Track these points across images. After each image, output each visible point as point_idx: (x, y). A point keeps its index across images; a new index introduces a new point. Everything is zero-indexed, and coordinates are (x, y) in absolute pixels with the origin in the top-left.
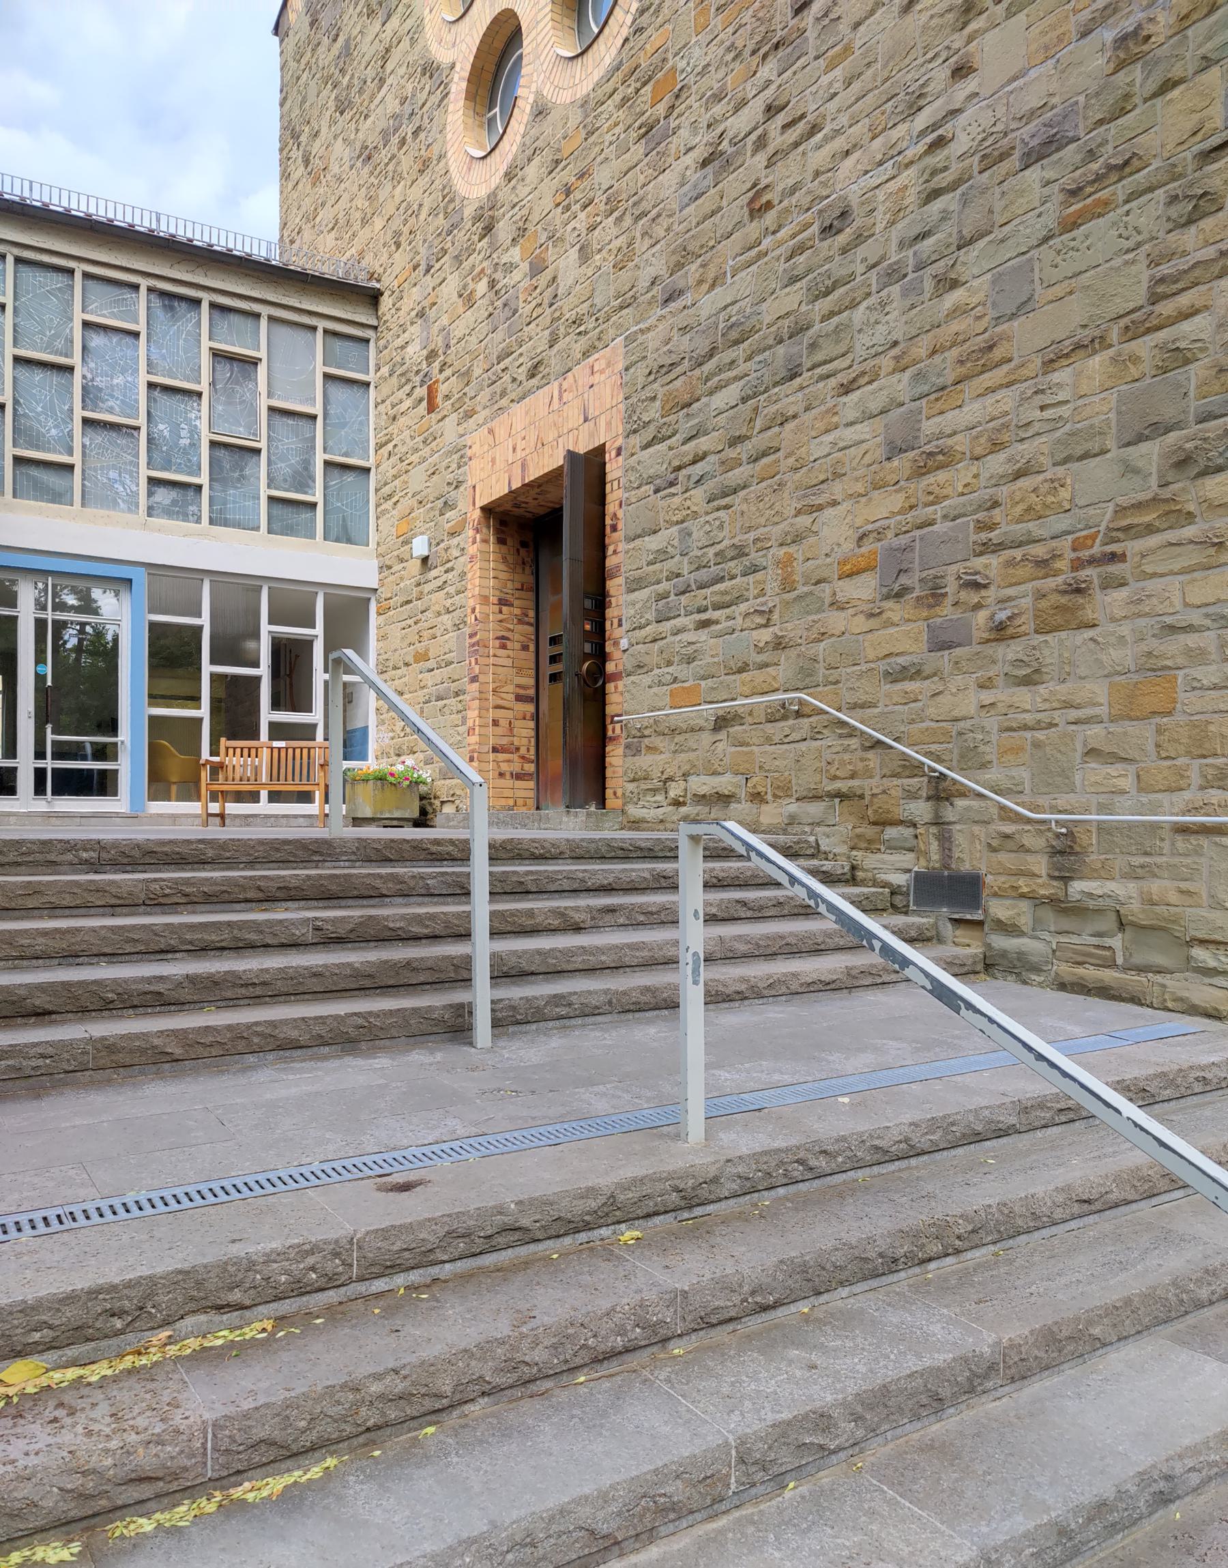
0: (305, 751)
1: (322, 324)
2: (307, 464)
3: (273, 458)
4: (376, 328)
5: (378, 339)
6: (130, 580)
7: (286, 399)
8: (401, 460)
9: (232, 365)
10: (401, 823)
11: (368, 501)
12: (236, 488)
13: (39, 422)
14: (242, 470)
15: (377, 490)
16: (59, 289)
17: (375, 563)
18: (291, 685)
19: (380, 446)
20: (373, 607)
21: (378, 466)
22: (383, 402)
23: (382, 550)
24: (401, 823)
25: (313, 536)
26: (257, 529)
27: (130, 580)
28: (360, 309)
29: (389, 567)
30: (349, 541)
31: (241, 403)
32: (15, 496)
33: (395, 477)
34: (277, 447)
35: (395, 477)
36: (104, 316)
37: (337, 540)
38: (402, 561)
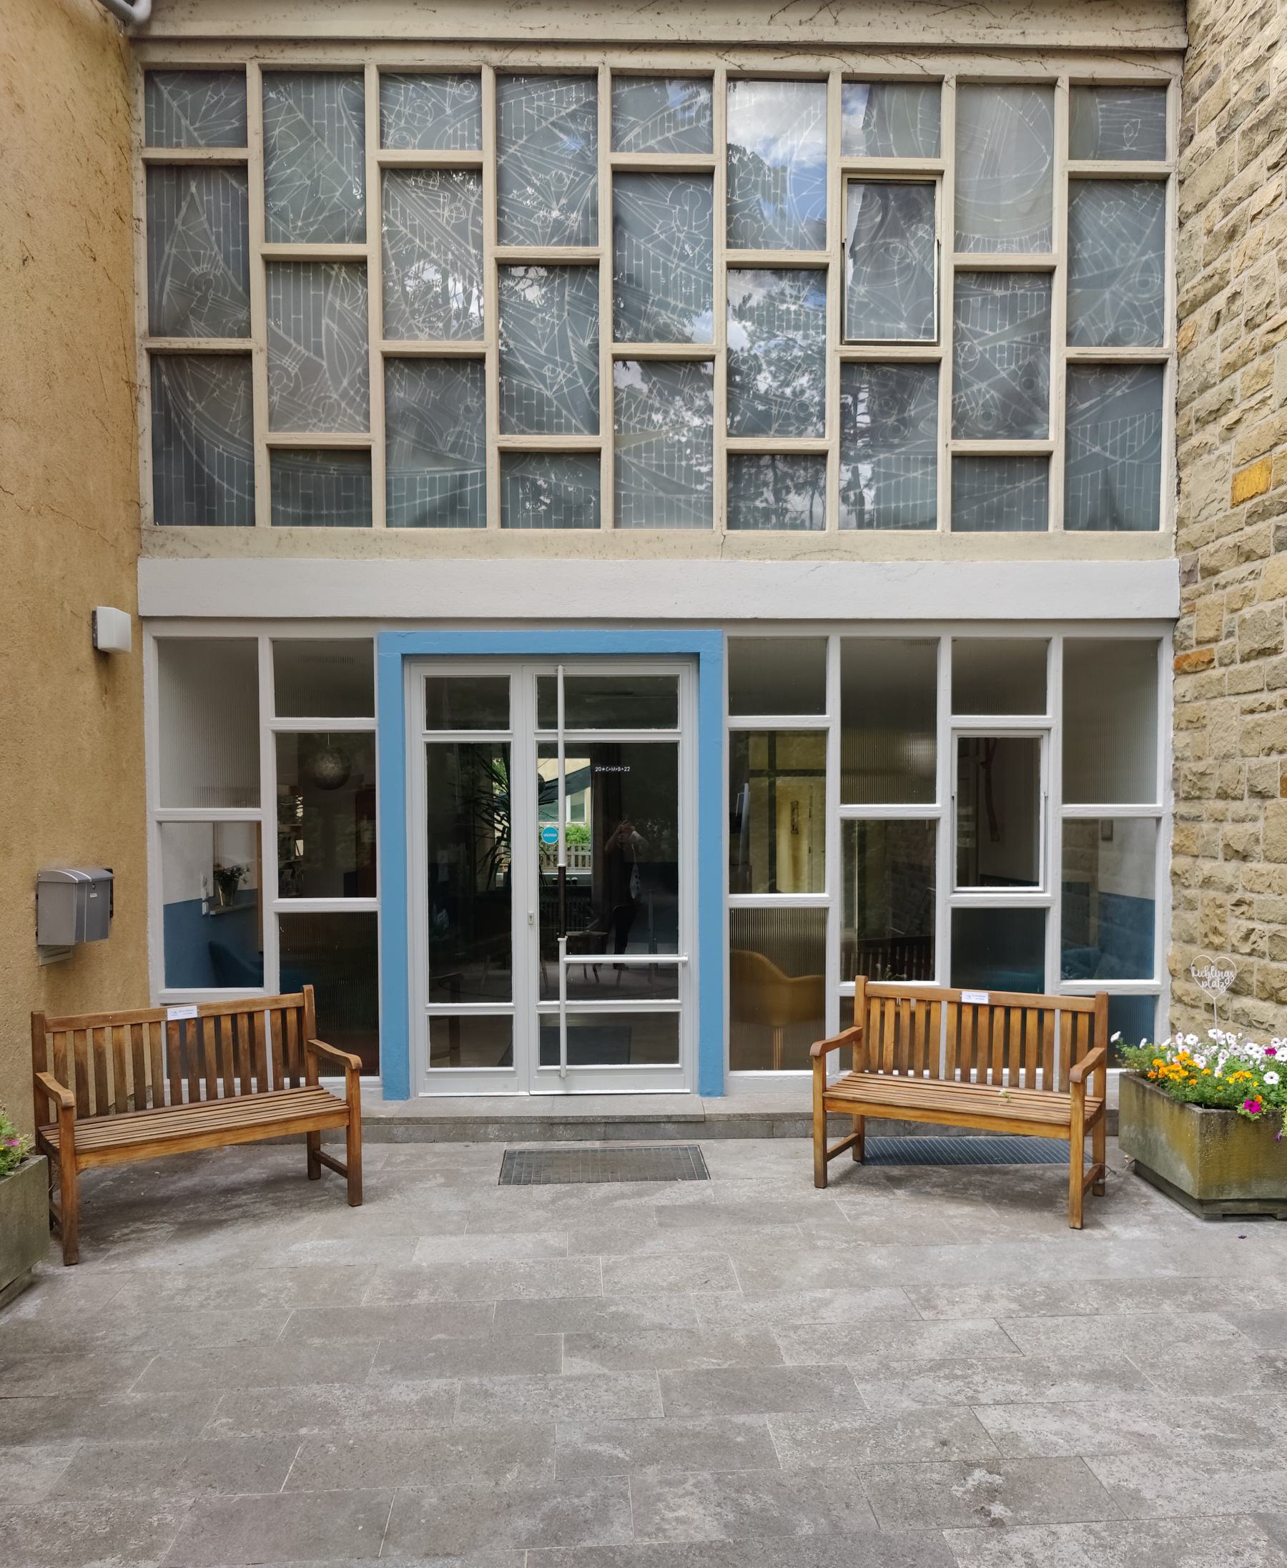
0: (1032, 1018)
1: (1065, 70)
2: (1032, 377)
3: (963, 374)
4: (1181, 54)
5: (1187, 76)
6: (697, 656)
7: (991, 246)
8: (1250, 325)
9: (885, 198)
10: (1269, 1208)
11: (1158, 434)
12: (892, 447)
13: (542, 379)
14: (902, 409)
15: (1179, 406)
16: (572, 116)
17: (1173, 564)
18: (988, 781)
19: (1187, 309)
20: (1167, 659)
21: (1183, 353)
22: (1200, 207)
23: (1192, 532)
24: (1269, 1208)
25: (1042, 524)
26: (931, 523)
27: (697, 656)
28: (1148, 22)
29: (1211, 572)
30: (1118, 523)
31: (902, 271)
32: (504, 525)
33: (1232, 367)
34: (971, 351)
35: (1232, 367)
36: (650, 150)
37: (1092, 525)
38: (1248, 557)
